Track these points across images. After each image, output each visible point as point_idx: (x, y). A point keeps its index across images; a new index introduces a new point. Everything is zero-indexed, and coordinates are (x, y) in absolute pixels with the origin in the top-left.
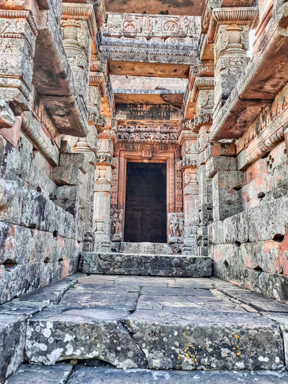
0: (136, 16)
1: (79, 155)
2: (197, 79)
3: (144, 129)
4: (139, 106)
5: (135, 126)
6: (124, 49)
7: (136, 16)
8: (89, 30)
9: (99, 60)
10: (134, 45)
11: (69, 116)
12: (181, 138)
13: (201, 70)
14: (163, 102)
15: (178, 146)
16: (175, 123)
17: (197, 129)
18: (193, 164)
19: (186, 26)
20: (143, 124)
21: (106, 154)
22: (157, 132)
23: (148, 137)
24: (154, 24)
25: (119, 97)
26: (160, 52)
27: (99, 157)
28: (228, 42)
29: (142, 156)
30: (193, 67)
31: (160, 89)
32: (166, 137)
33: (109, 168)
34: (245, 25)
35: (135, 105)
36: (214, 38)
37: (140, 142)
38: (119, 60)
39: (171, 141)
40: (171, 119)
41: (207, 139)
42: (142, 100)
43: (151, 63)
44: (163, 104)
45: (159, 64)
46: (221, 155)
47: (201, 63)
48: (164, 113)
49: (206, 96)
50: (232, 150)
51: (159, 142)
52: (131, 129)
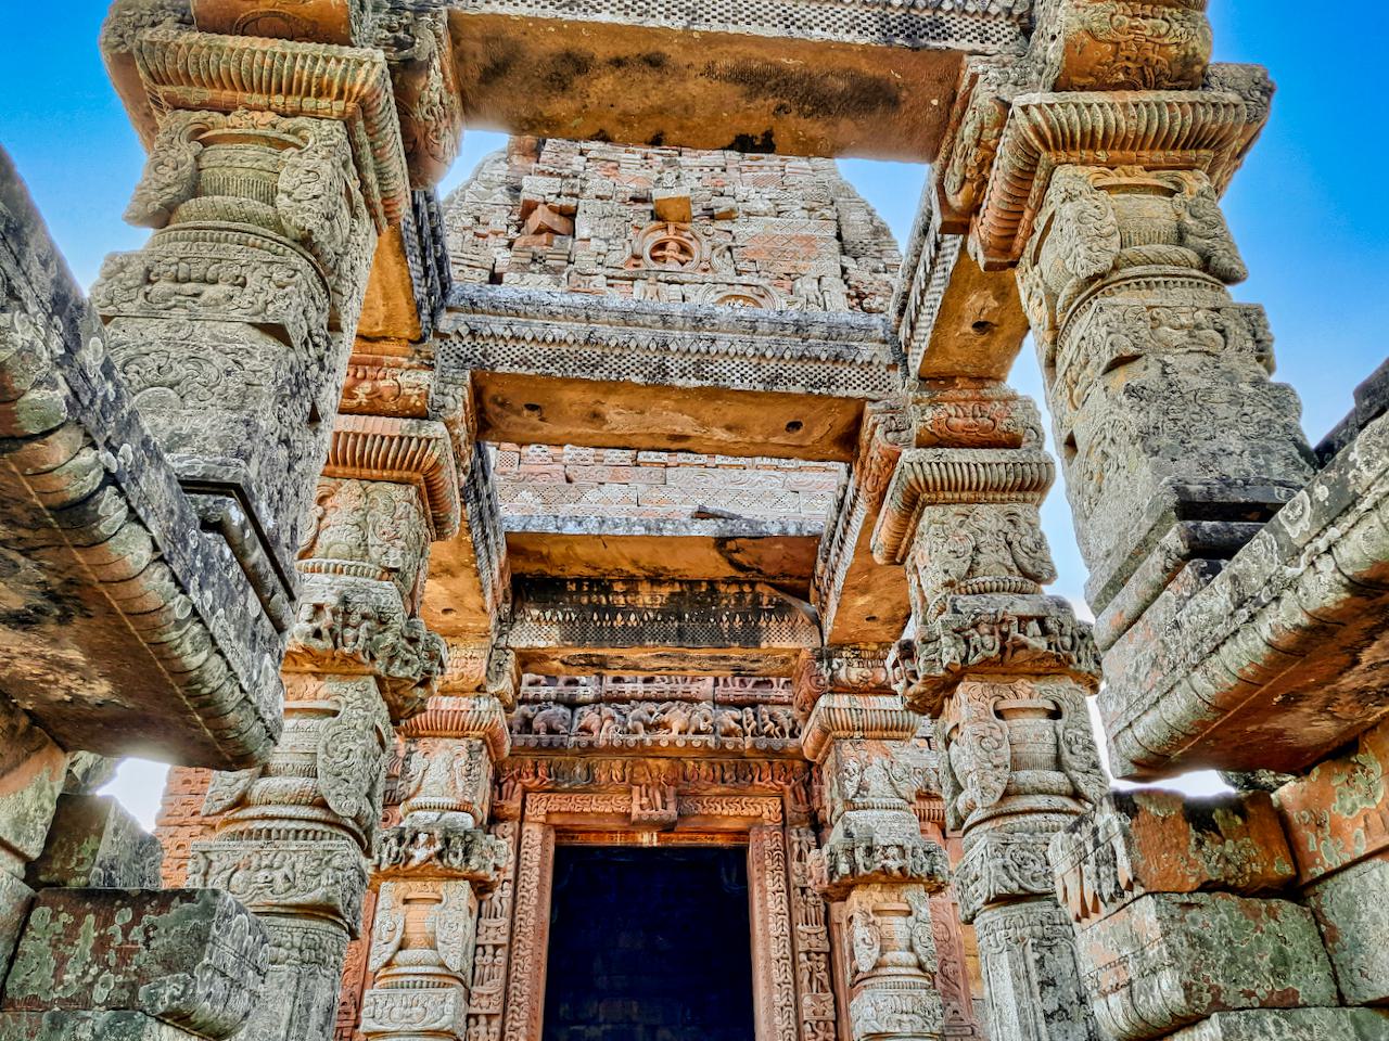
1: (177, 907)
2: (909, 455)
3: (640, 688)
4: (619, 587)
5: (601, 676)
9: (431, 367)
10: (604, 315)
11: (78, 621)
12: (816, 730)
13: (922, 419)
14: (729, 571)
15: (798, 764)
16: (785, 661)
17: (935, 694)
18: (890, 863)
20: (636, 668)
21: (449, 815)
22: (698, 702)
23: (658, 726)
25: (530, 548)
26: (722, 345)
27: (408, 837)
28: (1117, 239)
29: (627, 812)
30: (880, 406)
31: (714, 516)
32: (739, 722)
33: (461, 893)
34: (1191, 169)
35: (601, 585)
36: (1018, 242)
37: (622, 749)
38: (532, 372)
39: (763, 743)
40: (764, 645)
41: (1006, 750)
42: (635, 563)
43: (685, 391)
44: (729, 581)
45: (717, 393)
46: (1208, 887)
47: (920, 389)
48: (731, 618)
49: (963, 532)
50: (1265, 843)
51: (711, 744)
52: (581, 690)
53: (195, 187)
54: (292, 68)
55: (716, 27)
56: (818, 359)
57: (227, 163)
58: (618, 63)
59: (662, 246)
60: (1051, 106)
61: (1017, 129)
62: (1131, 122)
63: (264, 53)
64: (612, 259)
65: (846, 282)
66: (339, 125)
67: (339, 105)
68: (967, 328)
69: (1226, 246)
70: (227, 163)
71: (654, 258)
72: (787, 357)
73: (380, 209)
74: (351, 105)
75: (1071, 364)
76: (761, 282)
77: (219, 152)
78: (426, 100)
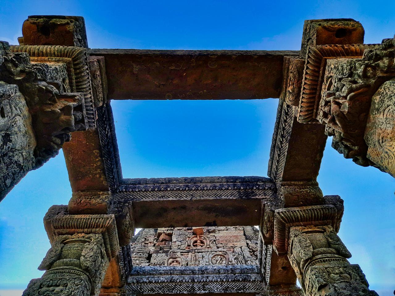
0: (181, 253)
6: (161, 279)
7: (181, 253)
8: (106, 247)
10: (175, 272)
19: (235, 259)
24: (200, 259)
26: (210, 278)
28: (311, 247)
34: (327, 225)
53: (60, 257)
54: (90, 222)
55: (198, 198)
56: (239, 280)
57: (69, 249)
58: (174, 209)
59: (196, 242)
60: (285, 212)
61: (277, 218)
62: (307, 214)
63: (84, 219)
64: (182, 247)
65: (249, 248)
66: (101, 235)
67: (101, 230)
68: (280, 269)
69: (343, 247)
70: (69, 249)
71: (194, 246)
72: (230, 281)
73: (110, 254)
74: (104, 229)
75: (309, 286)
76: (224, 250)
77: (68, 246)
78: (125, 224)
